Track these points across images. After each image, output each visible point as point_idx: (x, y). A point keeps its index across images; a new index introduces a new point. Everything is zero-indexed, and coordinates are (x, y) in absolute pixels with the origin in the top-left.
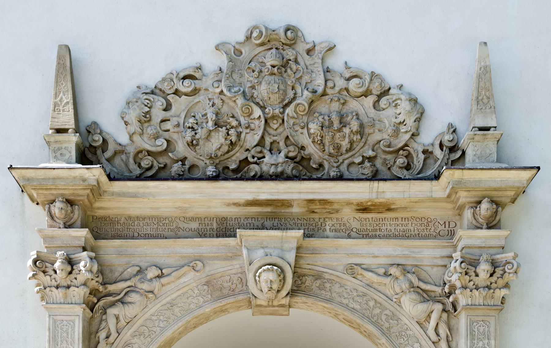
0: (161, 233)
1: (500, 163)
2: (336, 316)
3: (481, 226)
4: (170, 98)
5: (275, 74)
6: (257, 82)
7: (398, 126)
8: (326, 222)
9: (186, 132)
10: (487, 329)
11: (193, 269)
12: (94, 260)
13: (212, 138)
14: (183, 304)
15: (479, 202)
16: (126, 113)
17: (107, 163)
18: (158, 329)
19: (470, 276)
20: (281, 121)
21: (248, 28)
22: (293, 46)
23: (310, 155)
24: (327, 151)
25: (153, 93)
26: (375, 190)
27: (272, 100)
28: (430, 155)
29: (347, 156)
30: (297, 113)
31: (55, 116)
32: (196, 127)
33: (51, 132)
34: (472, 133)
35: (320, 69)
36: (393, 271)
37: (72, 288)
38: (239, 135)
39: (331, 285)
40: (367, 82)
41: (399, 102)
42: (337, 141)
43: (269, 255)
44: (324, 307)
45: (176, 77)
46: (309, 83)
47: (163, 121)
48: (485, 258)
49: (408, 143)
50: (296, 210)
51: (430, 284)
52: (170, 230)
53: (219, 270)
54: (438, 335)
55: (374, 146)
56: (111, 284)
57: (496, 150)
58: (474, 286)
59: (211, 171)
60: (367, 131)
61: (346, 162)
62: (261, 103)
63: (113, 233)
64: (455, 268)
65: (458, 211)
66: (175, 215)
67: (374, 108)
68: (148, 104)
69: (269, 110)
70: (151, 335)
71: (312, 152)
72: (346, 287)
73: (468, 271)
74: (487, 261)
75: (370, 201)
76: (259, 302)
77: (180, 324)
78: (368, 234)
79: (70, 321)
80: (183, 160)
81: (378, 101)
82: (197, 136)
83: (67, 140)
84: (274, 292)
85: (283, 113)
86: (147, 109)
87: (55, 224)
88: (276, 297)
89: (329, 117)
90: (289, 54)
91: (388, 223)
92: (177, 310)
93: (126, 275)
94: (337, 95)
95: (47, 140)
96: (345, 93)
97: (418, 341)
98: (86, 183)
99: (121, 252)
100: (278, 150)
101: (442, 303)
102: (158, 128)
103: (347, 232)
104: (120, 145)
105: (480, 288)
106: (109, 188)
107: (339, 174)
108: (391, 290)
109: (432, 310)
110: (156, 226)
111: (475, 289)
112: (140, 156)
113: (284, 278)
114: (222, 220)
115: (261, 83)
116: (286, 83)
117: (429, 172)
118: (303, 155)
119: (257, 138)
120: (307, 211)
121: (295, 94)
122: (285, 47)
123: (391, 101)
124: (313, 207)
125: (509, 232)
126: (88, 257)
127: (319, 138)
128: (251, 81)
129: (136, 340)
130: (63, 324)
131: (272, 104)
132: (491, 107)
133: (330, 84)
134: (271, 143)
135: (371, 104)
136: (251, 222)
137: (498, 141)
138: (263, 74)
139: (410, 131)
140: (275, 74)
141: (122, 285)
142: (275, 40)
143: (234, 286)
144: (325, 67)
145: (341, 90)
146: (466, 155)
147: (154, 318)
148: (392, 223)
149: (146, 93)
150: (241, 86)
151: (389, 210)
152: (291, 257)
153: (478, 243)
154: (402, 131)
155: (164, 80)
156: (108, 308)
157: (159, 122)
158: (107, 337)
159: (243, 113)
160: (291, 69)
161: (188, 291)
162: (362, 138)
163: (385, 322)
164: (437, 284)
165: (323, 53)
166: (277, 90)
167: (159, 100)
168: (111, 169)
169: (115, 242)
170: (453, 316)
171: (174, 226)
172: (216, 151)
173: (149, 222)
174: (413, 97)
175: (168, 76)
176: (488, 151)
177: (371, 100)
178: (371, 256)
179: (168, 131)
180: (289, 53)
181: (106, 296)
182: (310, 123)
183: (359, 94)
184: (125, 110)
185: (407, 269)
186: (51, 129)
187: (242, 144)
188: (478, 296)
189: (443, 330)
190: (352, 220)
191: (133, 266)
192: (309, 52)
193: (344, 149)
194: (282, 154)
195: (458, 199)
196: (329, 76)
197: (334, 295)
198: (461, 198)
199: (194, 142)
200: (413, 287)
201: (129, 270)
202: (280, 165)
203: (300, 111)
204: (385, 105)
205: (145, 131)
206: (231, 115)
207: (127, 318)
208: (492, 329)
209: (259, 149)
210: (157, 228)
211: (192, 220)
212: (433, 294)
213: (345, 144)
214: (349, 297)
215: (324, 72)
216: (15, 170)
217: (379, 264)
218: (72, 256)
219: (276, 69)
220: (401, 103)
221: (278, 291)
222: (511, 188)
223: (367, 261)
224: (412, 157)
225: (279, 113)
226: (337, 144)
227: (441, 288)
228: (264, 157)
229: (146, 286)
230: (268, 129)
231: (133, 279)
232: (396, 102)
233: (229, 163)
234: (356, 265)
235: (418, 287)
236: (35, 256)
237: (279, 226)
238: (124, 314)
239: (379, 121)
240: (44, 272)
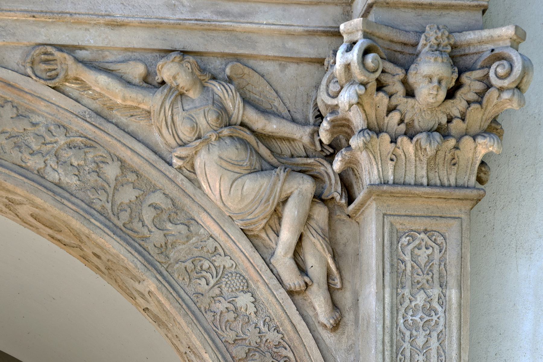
19: (390, 96)
48: (433, 40)
51: (278, 115)
54: (302, 270)
58: (403, 127)
64: (348, 67)
72: (35, 119)
73: (385, 79)
74: (437, 49)
97: (247, 289)
108: (164, 130)
109: (284, 195)
111: (405, 134)
163: (153, 229)
164: (298, 116)
170: (344, 217)
185: (211, 67)
188: (413, 157)
200: (229, 125)
208: (452, 256)
212: (286, 149)
214: (45, 149)
217: (127, 49)
227: (308, 130)
234: (61, 48)
235: (243, 124)
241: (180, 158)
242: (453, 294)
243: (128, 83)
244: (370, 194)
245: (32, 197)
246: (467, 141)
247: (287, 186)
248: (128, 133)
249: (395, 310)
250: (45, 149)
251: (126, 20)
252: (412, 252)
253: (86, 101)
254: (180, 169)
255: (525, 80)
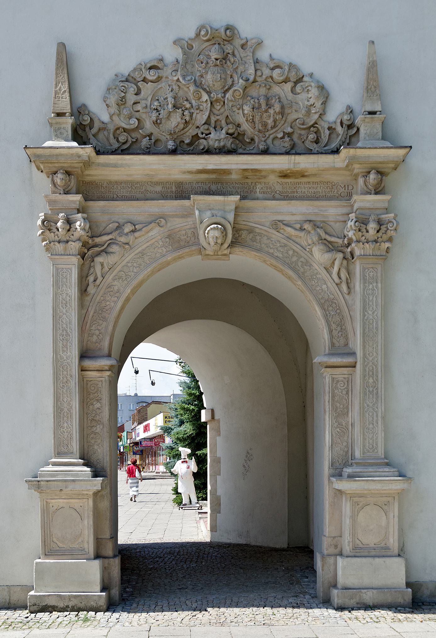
0: (134, 195)
1: (385, 140)
2: (265, 261)
3: (370, 192)
4: (139, 84)
5: (218, 65)
6: (205, 72)
7: (309, 107)
8: (257, 186)
9: (152, 112)
10: (375, 274)
11: (158, 225)
12: (86, 220)
13: (171, 117)
14: (151, 253)
15: (369, 172)
16: (108, 98)
17: (94, 138)
18: (133, 273)
19: (362, 232)
20: (222, 103)
21: (197, 27)
22: (231, 42)
23: (244, 131)
24: (257, 128)
25: (127, 80)
26: (292, 162)
27: (216, 86)
28: (334, 131)
29: (271, 132)
30: (234, 97)
31: (56, 102)
32: (159, 108)
33: (53, 115)
34: (363, 116)
35: (251, 61)
36: (307, 226)
37: (70, 243)
38: (191, 115)
39: (261, 238)
40: (286, 71)
41: (310, 88)
42: (265, 120)
43: (215, 215)
44: (256, 255)
45: (145, 68)
46: (243, 72)
47: (135, 103)
48: (373, 218)
49: (317, 122)
50: (234, 176)
51: (334, 236)
52: (140, 192)
53: (177, 226)
54: (340, 278)
55: (292, 123)
56: (97, 237)
57: (381, 130)
58: (366, 240)
59: (171, 145)
60: (287, 111)
61: (272, 137)
62: (208, 89)
63: (98, 195)
64: (351, 226)
65: (354, 177)
66: (145, 180)
67: (292, 92)
68: (124, 90)
69: (214, 95)
70: (127, 279)
71: (246, 128)
72: (272, 239)
73: (361, 228)
74: (374, 220)
75: (289, 169)
76: (207, 252)
77: (149, 270)
78: (288, 196)
79: (68, 268)
80: (150, 136)
81: (295, 86)
82: (161, 116)
83: (65, 122)
84: (219, 245)
85: (224, 97)
86: (123, 94)
87: (56, 190)
88: (220, 249)
89: (258, 100)
90: (229, 48)
91: (303, 186)
92: (146, 258)
93: (108, 229)
94: (264, 82)
95: (50, 122)
96: (270, 80)
97: (325, 284)
98: (81, 159)
99: (105, 211)
100: (221, 127)
101: (342, 252)
102: (132, 109)
103: (273, 194)
104: (103, 123)
105: (370, 242)
106: (96, 160)
107: (266, 147)
108: (305, 242)
109: (335, 258)
110: (130, 190)
111: (366, 242)
112: (118, 132)
113: (226, 235)
114: (179, 184)
115: (207, 73)
116: (226, 72)
117: (333, 146)
118: (239, 131)
119: (205, 117)
120: (242, 178)
121: (233, 81)
122: (226, 43)
123: (304, 87)
124: (247, 174)
125: (391, 197)
126: (82, 218)
127: (251, 118)
128: (200, 71)
129: (116, 283)
130: (63, 271)
131: (216, 90)
132: (377, 95)
133: (259, 73)
134: (215, 122)
135: (290, 89)
136: (200, 186)
137: (382, 123)
138: (209, 65)
139: (318, 112)
140: (218, 65)
141: (105, 238)
142: (218, 37)
143: (188, 239)
144: (255, 59)
145: (267, 77)
146: (360, 131)
147: (129, 265)
148: (306, 186)
149: (122, 81)
150: (193, 75)
151: (303, 176)
152: (231, 217)
153: (368, 205)
154: (313, 112)
155: (135, 70)
156: (95, 257)
157: (132, 105)
158: (95, 281)
159: (195, 97)
160: (230, 61)
161: (154, 242)
162: (283, 117)
163: (301, 268)
164: (339, 236)
165: (253, 47)
166: (220, 79)
167: (132, 87)
168: (96, 143)
169: (99, 203)
170: (351, 263)
171: (144, 189)
172: (174, 128)
173: (125, 186)
174: (320, 84)
175: (138, 67)
176: (375, 131)
177: (289, 86)
178: (290, 213)
179: (138, 111)
180: (228, 48)
181: (93, 247)
182: (244, 105)
183: (281, 81)
184: (107, 95)
185: (317, 224)
186: (53, 113)
187: (193, 122)
188: (368, 248)
189: (344, 275)
190: (276, 184)
191: (113, 222)
192: (243, 46)
193: (270, 126)
194: (224, 131)
195: (354, 169)
196: (258, 66)
197: (263, 245)
198: (355, 169)
199: (158, 121)
200: (321, 240)
201: (110, 225)
202: (222, 140)
203: (237, 96)
204: (300, 90)
205: (121, 112)
206: (186, 99)
207: (109, 264)
208: (379, 275)
209: (206, 127)
210: (131, 191)
211: (157, 184)
212: (336, 245)
213: (270, 122)
214: (274, 247)
215: (254, 63)
216: (29, 149)
217: (296, 221)
218: (70, 217)
219: (218, 61)
220: (312, 89)
221: (222, 244)
222: (392, 162)
223: (287, 218)
224: (320, 133)
225: (221, 98)
226: (265, 122)
227: (342, 240)
228: (210, 133)
229: (123, 239)
230: (213, 110)
231: (114, 234)
232: (308, 88)
233: (184, 138)
234: (279, 221)
235: (325, 239)
236: (43, 217)
237: (222, 189)
238: (107, 262)
239: (295, 103)
240: (50, 230)
241: (308, 248)
242: (379, 285)
243: (296, 229)
244: (357, 258)
245: (270, 260)
246: (383, 243)
247: (336, 255)
248: (295, 242)
249: (364, 290)
250: (274, 247)
251: (296, 213)
252: (368, 273)
253: (285, 234)
254: (308, 251)
255: (397, 228)
